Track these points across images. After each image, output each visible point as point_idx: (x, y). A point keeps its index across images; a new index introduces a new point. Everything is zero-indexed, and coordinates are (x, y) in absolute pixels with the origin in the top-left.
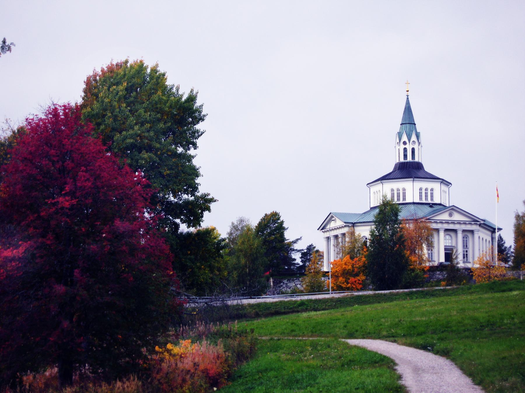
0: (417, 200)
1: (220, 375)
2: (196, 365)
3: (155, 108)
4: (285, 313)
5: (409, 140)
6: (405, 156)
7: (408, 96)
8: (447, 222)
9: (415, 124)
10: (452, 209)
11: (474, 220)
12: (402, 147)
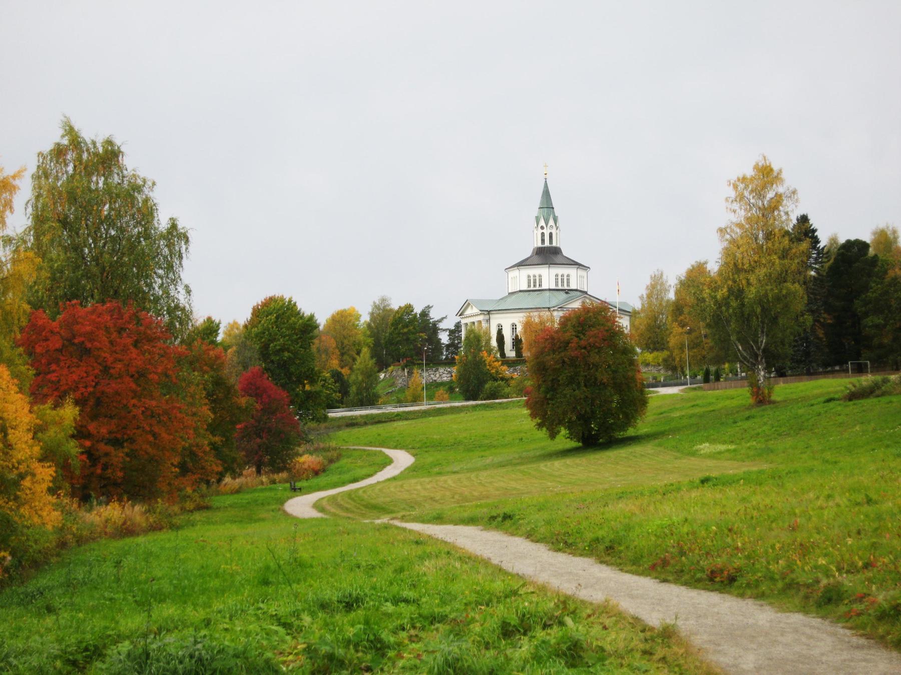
0: (553, 287)
1: (319, 470)
2: (309, 466)
3: (292, 327)
4: (385, 422)
5: (547, 225)
6: (543, 241)
9: (553, 208)
12: (540, 231)
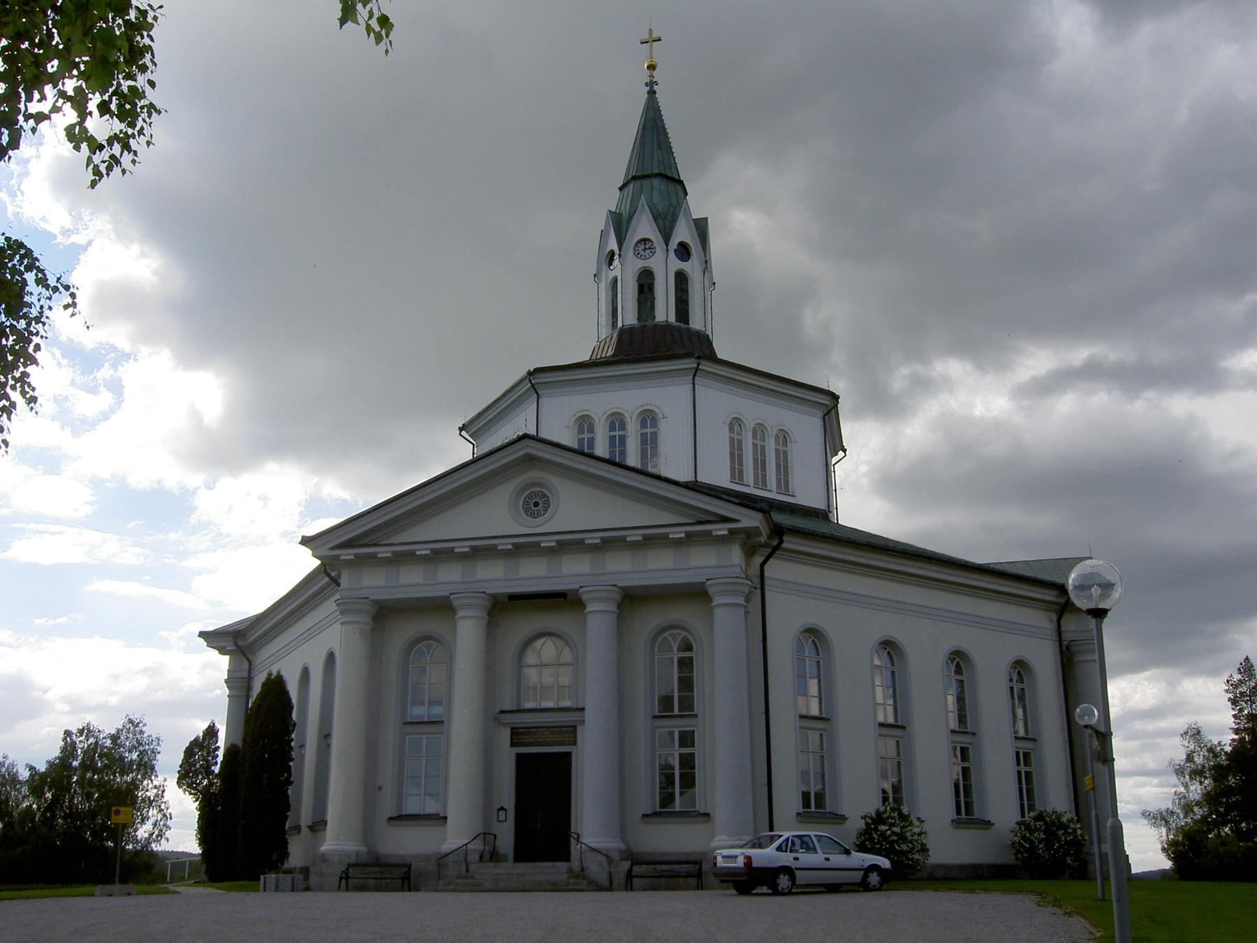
8: (523, 549)
10: (530, 460)
11: (704, 517)
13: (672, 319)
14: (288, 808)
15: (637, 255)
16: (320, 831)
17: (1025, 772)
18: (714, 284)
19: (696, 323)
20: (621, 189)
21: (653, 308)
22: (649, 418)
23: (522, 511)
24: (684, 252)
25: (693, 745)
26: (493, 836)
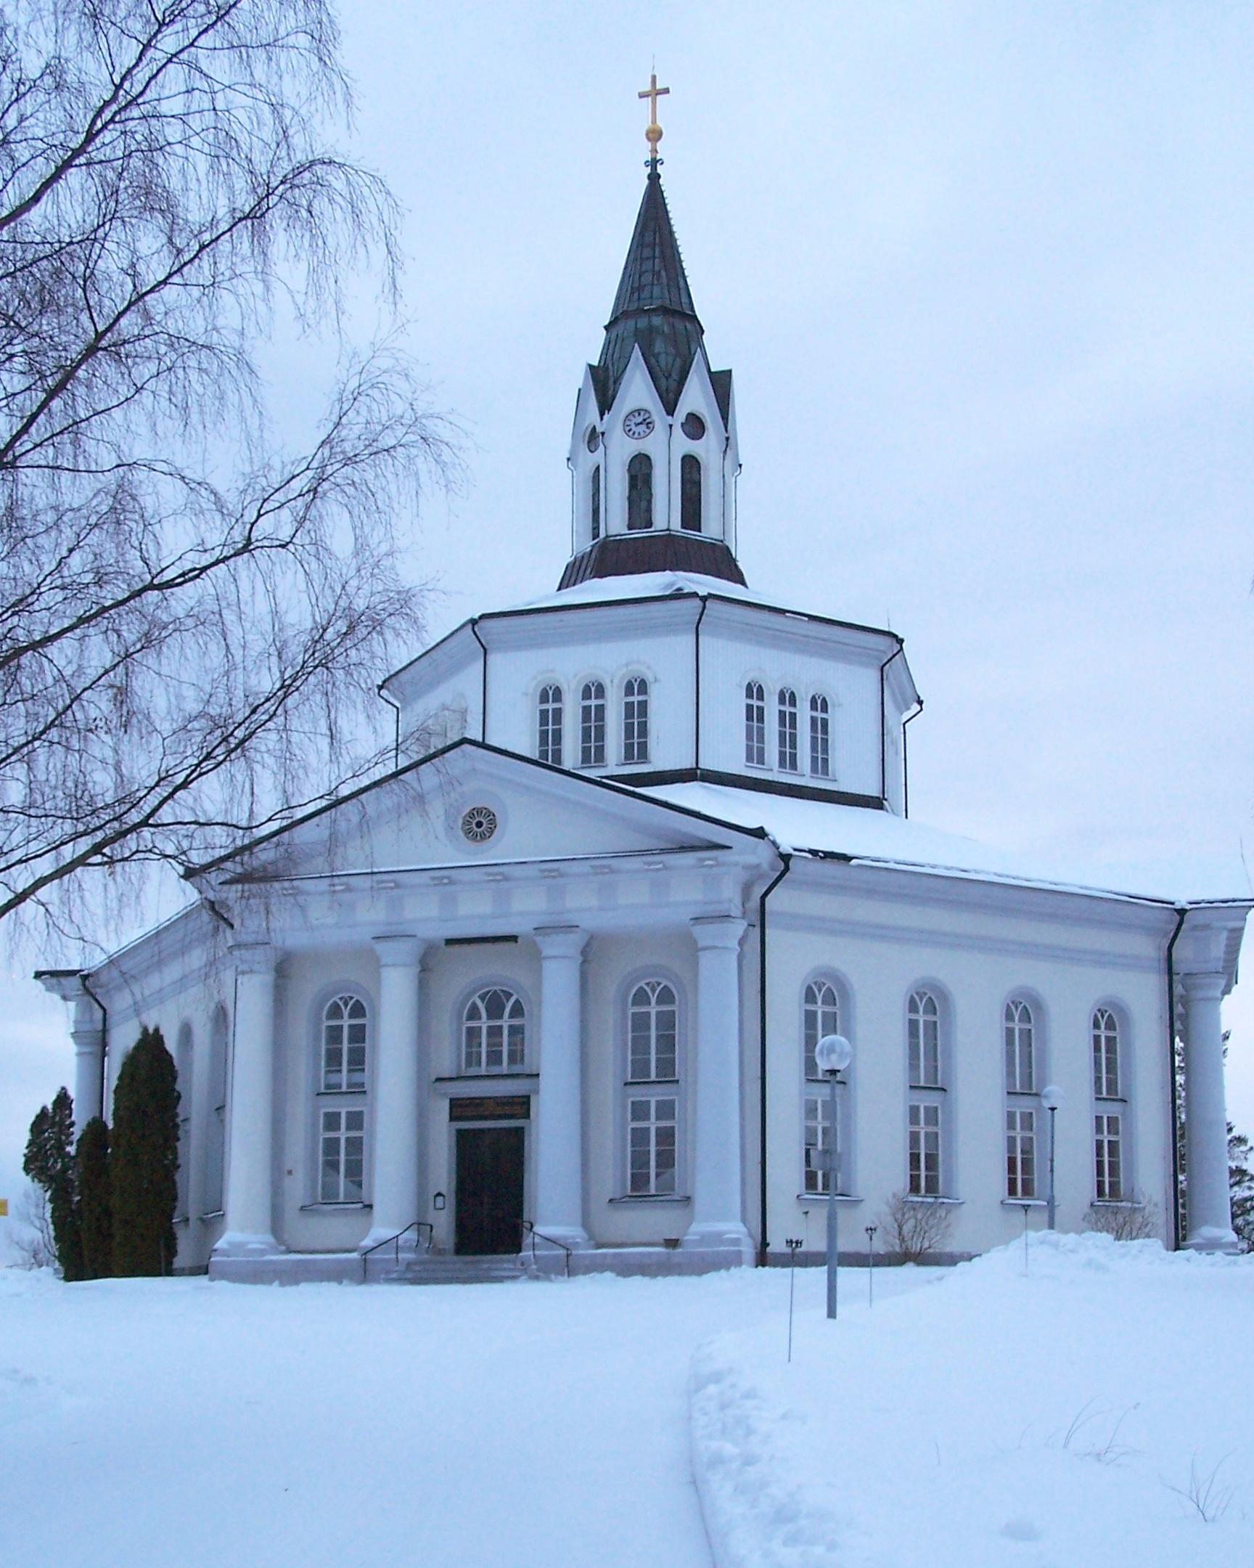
7: (655, 135)
13: (676, 524)
14: (175, 1199)
15: (628, 432)
16: (1208, 999)
17: (1109, 1141)
18: (740, 466)
19: (710, 529)
20: (606, 328)
21: (649, 510)
22: (636, 686)
23: (461, 834)
24: (695, 426)
25: (673, 1117)
26: (429, 1227)
